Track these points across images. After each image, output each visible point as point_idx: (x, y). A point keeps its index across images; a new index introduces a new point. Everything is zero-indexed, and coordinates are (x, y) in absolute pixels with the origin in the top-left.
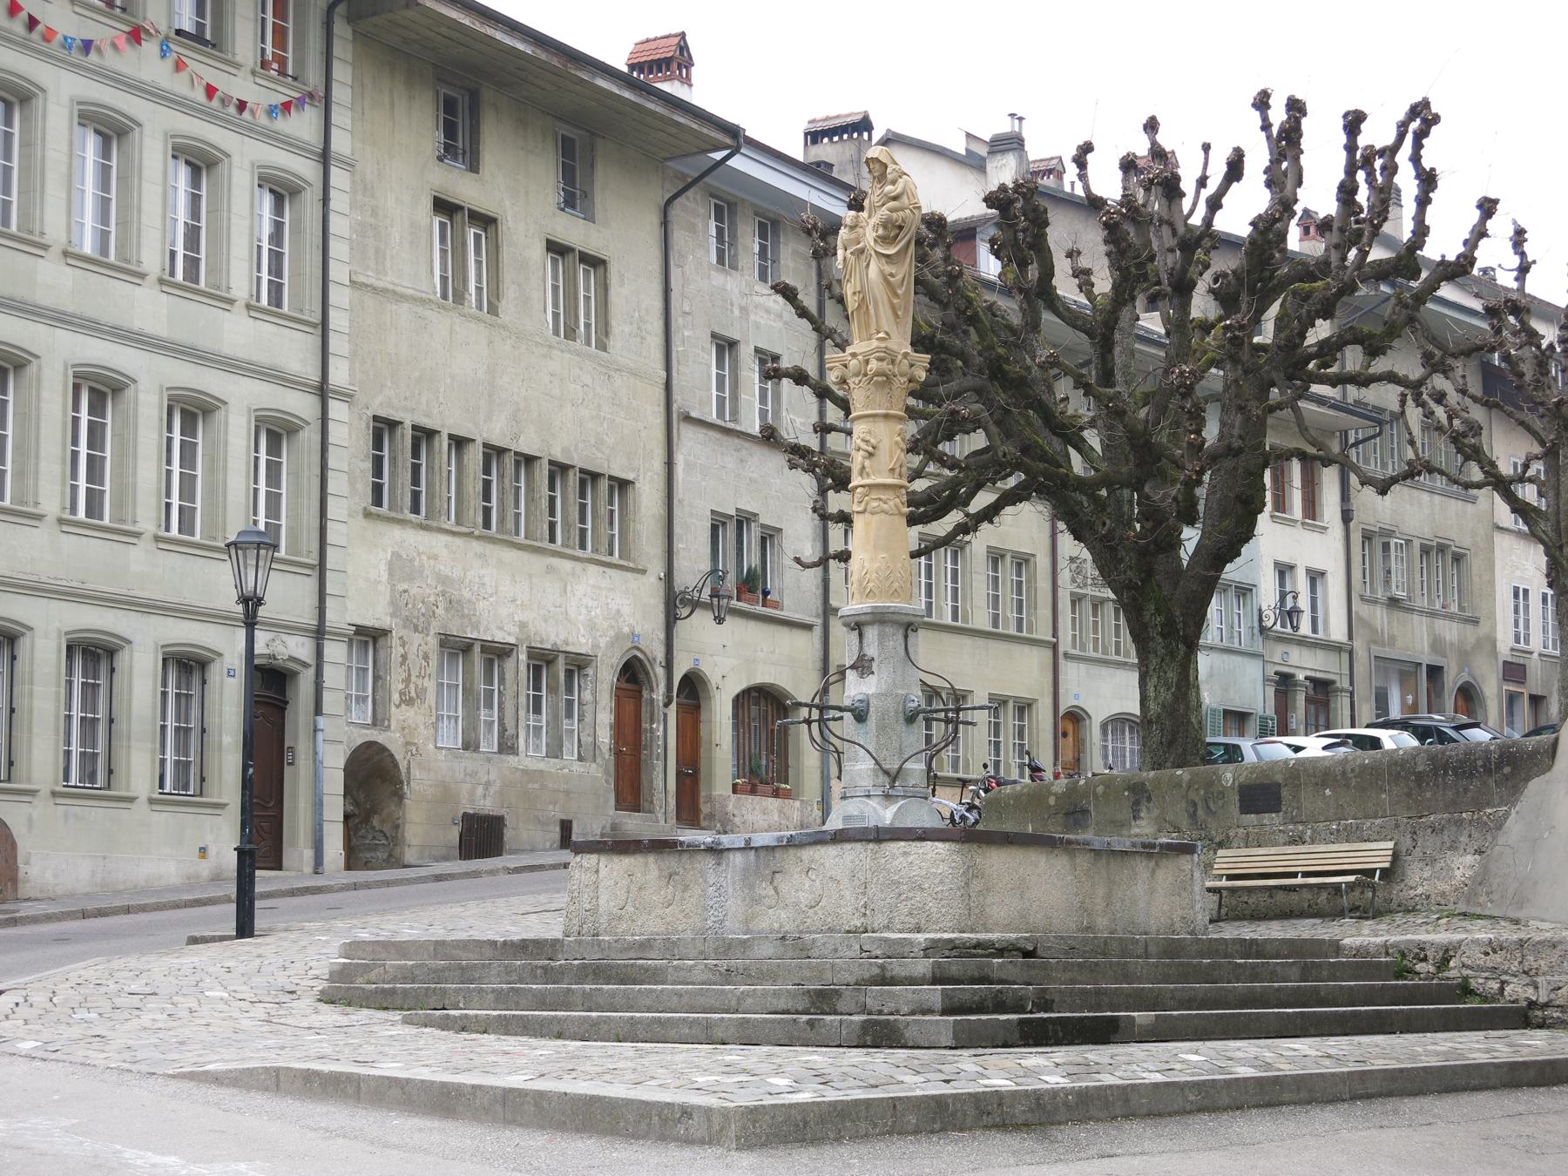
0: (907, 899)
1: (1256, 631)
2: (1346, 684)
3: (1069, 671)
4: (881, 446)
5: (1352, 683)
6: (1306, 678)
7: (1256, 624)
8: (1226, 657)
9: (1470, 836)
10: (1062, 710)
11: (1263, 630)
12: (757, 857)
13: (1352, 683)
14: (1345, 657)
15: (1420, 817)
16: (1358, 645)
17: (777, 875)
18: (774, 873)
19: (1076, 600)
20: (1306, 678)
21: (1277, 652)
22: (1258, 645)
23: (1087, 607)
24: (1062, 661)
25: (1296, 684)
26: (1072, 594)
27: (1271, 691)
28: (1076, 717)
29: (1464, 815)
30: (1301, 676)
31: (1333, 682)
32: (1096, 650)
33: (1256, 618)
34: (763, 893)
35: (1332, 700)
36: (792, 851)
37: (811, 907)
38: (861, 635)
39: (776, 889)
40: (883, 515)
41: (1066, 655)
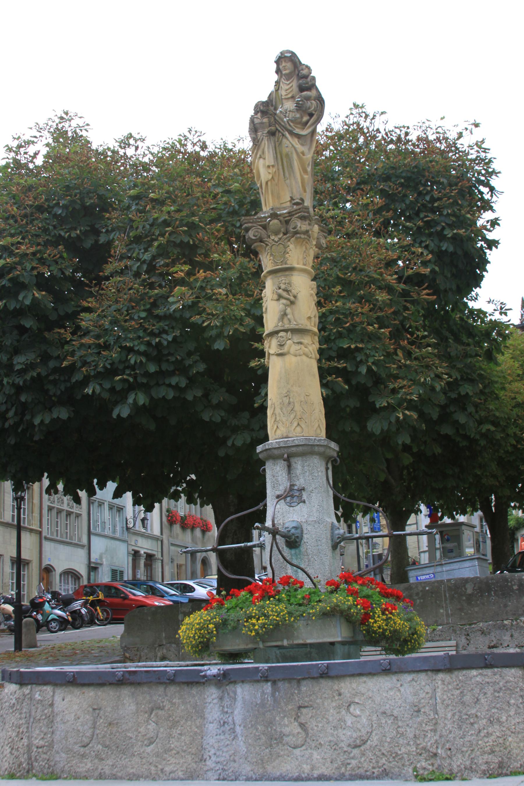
0: (488, 735)
1: (125, 529)
2: (160, 556)
3: (47, 546)
4: (299, 296)
5: (162, 556)
6: (145, 553)
7: (125, 526)
8: (113, 542)
9: (512, 636)
10: (43, 566)
11: (128, 529)
12: (275, 689)
13: (162, 556)
14: (159, 543)
15: (470, 625)
16: (165, 537)
17: (304, 711)
18: (300, 707)
19: (50, 509)
20: (145, 553)
21: (133, 539)
22: (126, 536)
23: (54, 512)
24: (44, 541)
25: (140, 556)
26: (49, 506)
27: (130, 559)
28: (48, 570)
29: (506, 622)
30: (142, 552)
31: (154, 555)
32: (57, 536)
33: (125, 523)
34: (286, 730)
35: (153, 563)
36: (325, 684)
37: (356, 746)
38: (289, 466)
39: (302, 725)
40: (304, 358)
41: (46, 538)
